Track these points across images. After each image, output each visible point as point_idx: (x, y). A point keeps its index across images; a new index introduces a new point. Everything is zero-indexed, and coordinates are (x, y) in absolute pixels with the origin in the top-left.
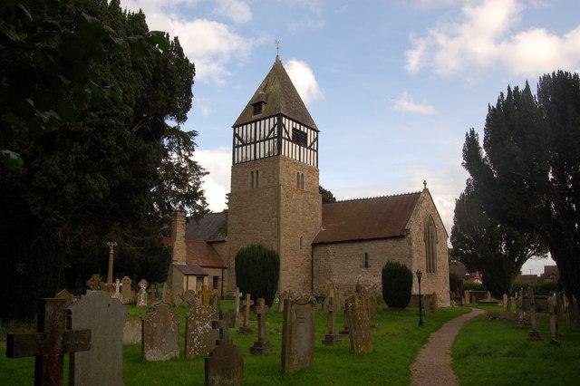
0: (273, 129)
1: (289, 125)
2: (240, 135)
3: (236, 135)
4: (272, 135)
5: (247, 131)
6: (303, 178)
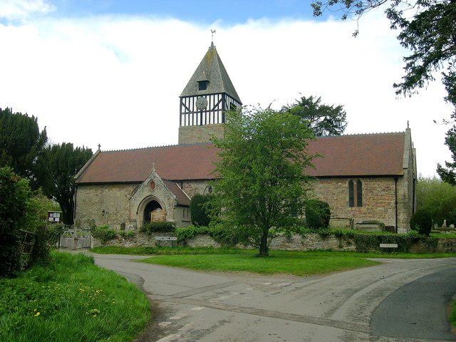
0: (218, 105)
1: (229, 100)
2: (187, 106)
3: (182, 104)
4: (216, 108)
5: (192, 103)
6: (351, 199)
